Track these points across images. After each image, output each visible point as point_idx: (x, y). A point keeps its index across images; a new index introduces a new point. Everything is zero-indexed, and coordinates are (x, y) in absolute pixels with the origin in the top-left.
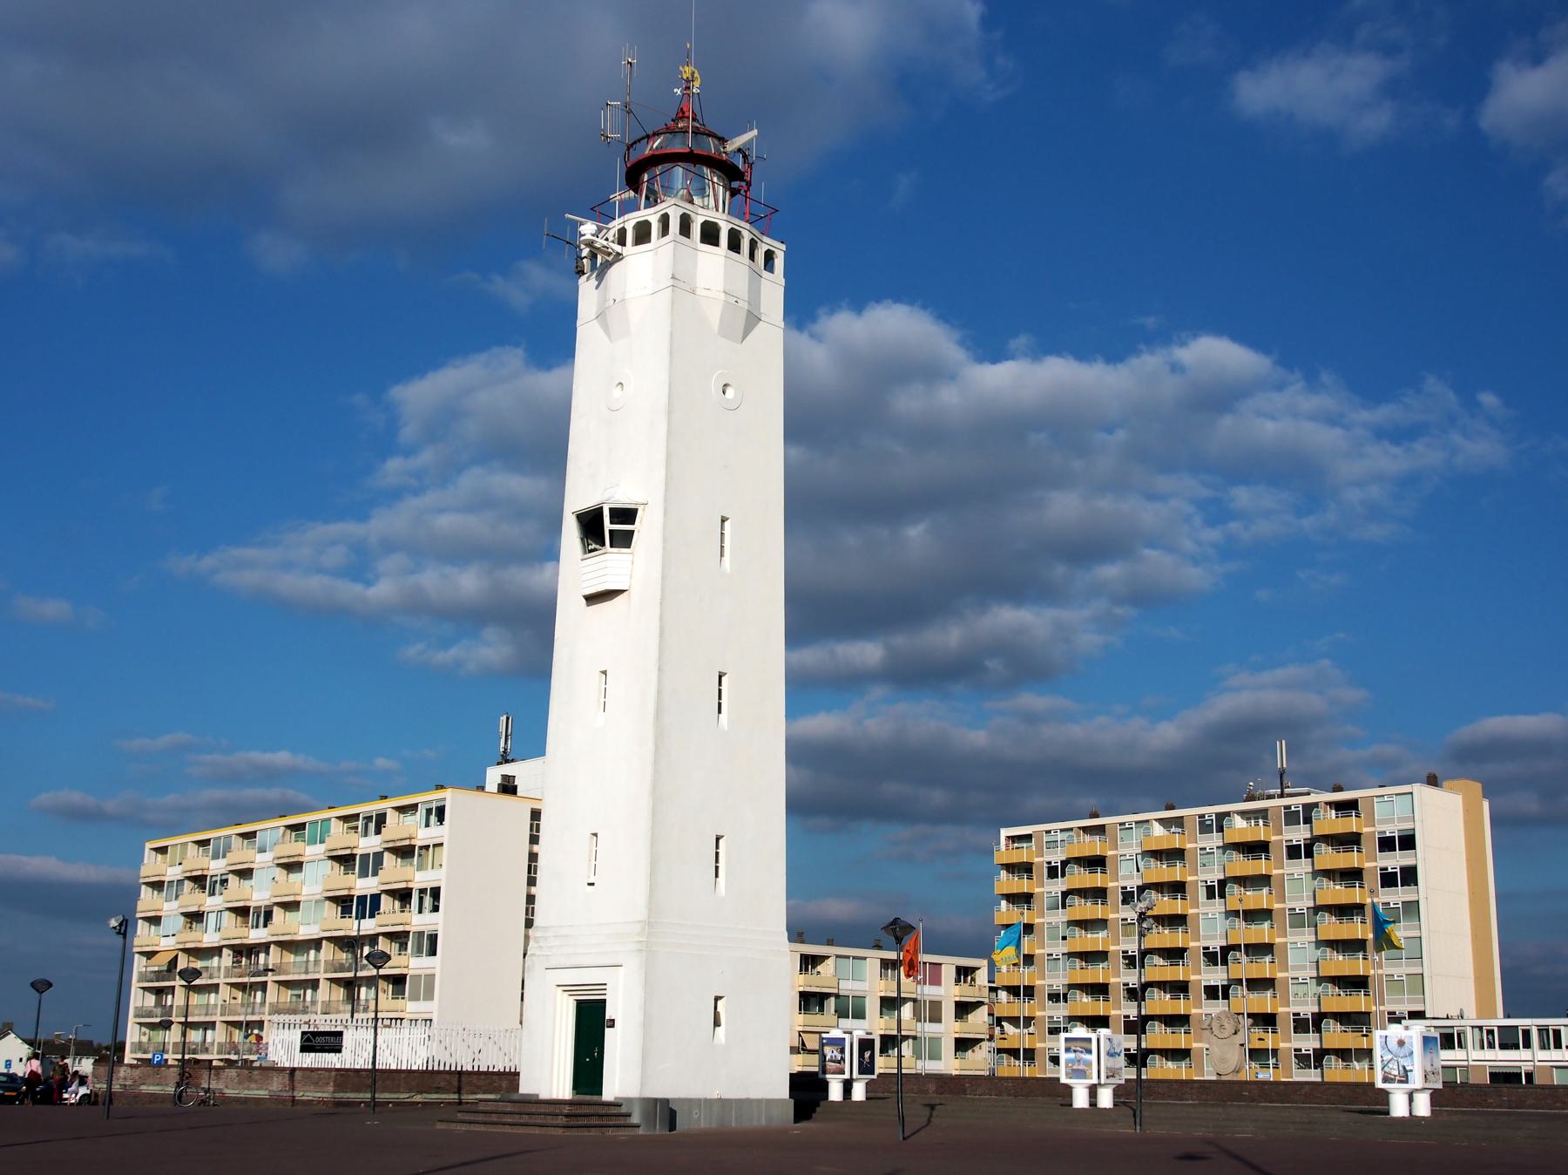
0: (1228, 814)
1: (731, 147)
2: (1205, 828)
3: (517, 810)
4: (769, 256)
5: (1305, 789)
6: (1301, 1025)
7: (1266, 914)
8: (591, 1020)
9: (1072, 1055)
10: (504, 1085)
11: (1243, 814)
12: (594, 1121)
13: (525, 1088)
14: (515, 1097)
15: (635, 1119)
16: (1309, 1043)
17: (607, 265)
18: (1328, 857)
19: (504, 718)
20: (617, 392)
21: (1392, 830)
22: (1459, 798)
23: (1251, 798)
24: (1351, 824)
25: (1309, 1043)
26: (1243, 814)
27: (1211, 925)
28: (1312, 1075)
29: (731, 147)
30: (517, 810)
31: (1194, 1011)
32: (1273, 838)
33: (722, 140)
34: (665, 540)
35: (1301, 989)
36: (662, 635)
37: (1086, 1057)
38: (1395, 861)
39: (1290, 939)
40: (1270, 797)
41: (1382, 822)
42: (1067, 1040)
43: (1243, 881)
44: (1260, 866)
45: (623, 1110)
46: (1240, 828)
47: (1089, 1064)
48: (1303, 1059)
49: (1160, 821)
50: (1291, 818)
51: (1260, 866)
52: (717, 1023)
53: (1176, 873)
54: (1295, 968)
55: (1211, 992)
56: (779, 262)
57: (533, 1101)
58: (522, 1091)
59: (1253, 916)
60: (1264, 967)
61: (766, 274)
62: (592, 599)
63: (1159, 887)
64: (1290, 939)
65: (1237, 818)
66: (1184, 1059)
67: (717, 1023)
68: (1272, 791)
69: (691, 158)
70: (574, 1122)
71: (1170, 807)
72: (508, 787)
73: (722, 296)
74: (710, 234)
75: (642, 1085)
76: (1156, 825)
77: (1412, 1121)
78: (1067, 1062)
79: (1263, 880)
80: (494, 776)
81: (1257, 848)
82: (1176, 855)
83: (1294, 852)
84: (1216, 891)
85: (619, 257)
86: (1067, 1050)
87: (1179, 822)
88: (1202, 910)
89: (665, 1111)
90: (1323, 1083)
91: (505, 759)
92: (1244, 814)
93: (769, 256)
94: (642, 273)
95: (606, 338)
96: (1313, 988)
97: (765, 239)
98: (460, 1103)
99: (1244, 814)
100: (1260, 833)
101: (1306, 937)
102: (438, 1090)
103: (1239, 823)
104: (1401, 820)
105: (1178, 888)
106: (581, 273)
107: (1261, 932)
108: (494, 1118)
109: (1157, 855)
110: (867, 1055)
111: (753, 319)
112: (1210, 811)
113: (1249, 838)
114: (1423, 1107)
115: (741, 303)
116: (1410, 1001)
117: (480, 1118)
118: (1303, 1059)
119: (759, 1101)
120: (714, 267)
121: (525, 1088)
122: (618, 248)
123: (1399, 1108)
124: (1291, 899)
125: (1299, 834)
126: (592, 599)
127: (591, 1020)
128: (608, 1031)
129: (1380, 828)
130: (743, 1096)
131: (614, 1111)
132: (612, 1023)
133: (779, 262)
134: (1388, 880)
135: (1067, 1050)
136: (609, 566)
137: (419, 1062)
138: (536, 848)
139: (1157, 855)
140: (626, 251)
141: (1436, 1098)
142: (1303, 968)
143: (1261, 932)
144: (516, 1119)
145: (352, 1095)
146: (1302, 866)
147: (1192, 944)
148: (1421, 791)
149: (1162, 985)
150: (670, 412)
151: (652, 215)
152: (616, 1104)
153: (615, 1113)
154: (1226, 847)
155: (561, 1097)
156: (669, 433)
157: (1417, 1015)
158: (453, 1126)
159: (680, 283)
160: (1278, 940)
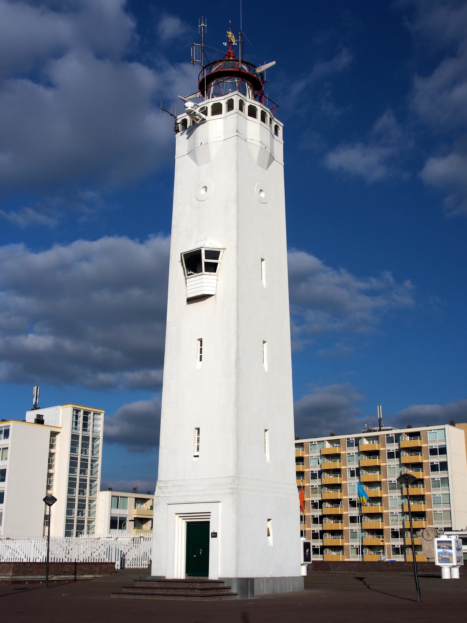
0: (360, 438)
1: (258, 71)
2: (350, 444)
3: (43, 433)
4: (276, 127)
5: (390, 428)
6: (395, 534)
7: (379, 483)
8: (198, 536)
9: (441, 550)
10: (97, 569)
11: (367, 438)
12: (214, 592)
13: (155, 573)
14: (149, 578)
15: (234, 590)
16: (398, 542)
17: (195, 125)
18: (407, 458)
19: (35, 388)
20: (203, 192)
21: (435, 445)
22: (463, 432)
23: (370, 431)
24: (417, 443)
25: (398, 542)
26: (367, 438)
27: (351, 488)
28: (400, 558)
29: (258, 71)
30: (43, 433)
31: (345, 528)
32: (381, 449)
33: (255, 67)
34: (238, 268)
35: (395, 518)
36: (238, 319)
37: (449, 551)
38: (437, 459)
39: (389, 495)
40: (375, 431)
41: (431, 442)
42: (438, 542)
43: (367, 468)
44: (376, 462)
45: (225, 585)
46: (366, 444)
47: (451, 555)
48: (396, 551)
49: (329, 441)
50: (390, 440)
51: (376, 462)
52: (269, 535)
53: (336, 464)
54: (392, 508)
55: (353, 520)
56: (280, 132)
57: (161, 580)
58: (152, 575)
59: (370, 484)
60: (377, 508)
61: (275, 136)
62: (190, 300)
63: (328, 471)
64: (389, 495)
65: (365, 440)
66: (339, 550)
67: (269, 535)
68: (375, 428)
69: (240, 74)
70: (204, 593)
71: (332, 435)
72: (40, 421)
73: (259, 144)
74: (252, 112)
75: (237, 570)
76: (327, 443)
77: (452, 581)
78: (439, 554)
79: (378, 468)
80: (31, 416)
81: (374, 454)
82: (337, 456)
83: (391, 455)
84: (355, 473)
85: (203, 121)
86: (439, 547)
87: (338, 441)
88: (348, 482)
89: (247, 584)
90: (405, 562)
91: (36, 407)
92: (368, 438)
93: (276, 127)
94: (216, 129)
95: (196, 165)
96: (400, 518)
97: (275, 119)
98: (75, 580)
99: (368, 438)
100: (376, 446)
101: (397, 493)
102: (65, 573)
103: (366, 442)
104: (440, 441)
105: (337, 472)
106: (177, 131)
107: (376, 492)
108: (149, 591)
109: (328, 456)
110: (307, 551)
111: (272, 159)
112: (353, 436)
113: (371, 449)
114: (456, 574)
115: (267, 149)
116: (445, 523)
117: (139, 591)
118: (396, 551)
119: (289, 578)
120: (255, 129)
121: (155, 573)
122: (204, 116)
123: (446, 575)
124: (390, 477)
125: (393, 447)
126: (190, 300)
127: (198, 536)
128: (212, 540)
129: (430, 444)
130: (282, 576)
131: (221, 585)
132: (215, 535)
133: (280, 132)
134: (434, 468)
135: (439, 547)
136: (203, 282)
137: (41, 557)
138: (52, 451)
139: (328, 456)
140: (207, 118)
141: (461, 569)
142: (396, 508)
143: (376, 492)
144: (165, 591)
145: (63, 577)
146: (395, 462)
147: (344, 497)
148: (448, 427)
149: (330, 516)
150: (238, 200)
151: (223, 100)
152: (220, 582)
153: (220, 586)
154: (360, 453)
155: (179, 577)
156: (238, 211)
157: (450, 529)
158: (122, 596)
159: (239, 134)
160: (384, 495)
